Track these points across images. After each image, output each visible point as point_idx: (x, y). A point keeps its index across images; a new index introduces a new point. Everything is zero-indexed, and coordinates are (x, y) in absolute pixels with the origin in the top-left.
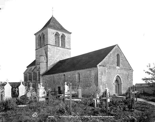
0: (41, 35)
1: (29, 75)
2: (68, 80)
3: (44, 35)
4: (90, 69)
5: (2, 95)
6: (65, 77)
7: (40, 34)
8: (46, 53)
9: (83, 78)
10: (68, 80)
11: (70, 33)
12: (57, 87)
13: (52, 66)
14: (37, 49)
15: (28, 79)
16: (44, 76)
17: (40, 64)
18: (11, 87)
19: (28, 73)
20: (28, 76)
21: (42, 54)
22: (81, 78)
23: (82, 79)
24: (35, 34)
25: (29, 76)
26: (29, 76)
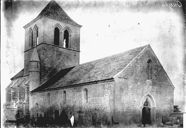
0: (33, 29)
1: (14, 92)
2: (70, 100)
3: (38, 29)
4: (103, 83)
5: (102, 5)
6: (66, 96)
7: (32, 26)
8: (95, 5)
9: (93, 97)
10: (70, 100)
11: (80, 26)
12: (54, 111)
13: (183, 11)
14: (27, 51)
15: (12, 98)
16: (35, 93)
17: (29, 75)
18: (22, 67)
19: (12, 89)
20: (12, 94)
21: (33, 60)
22: (89, 97)
23: (91, 99)
24: (25, 27)
25: (13, 93)
26: (13, 93)
